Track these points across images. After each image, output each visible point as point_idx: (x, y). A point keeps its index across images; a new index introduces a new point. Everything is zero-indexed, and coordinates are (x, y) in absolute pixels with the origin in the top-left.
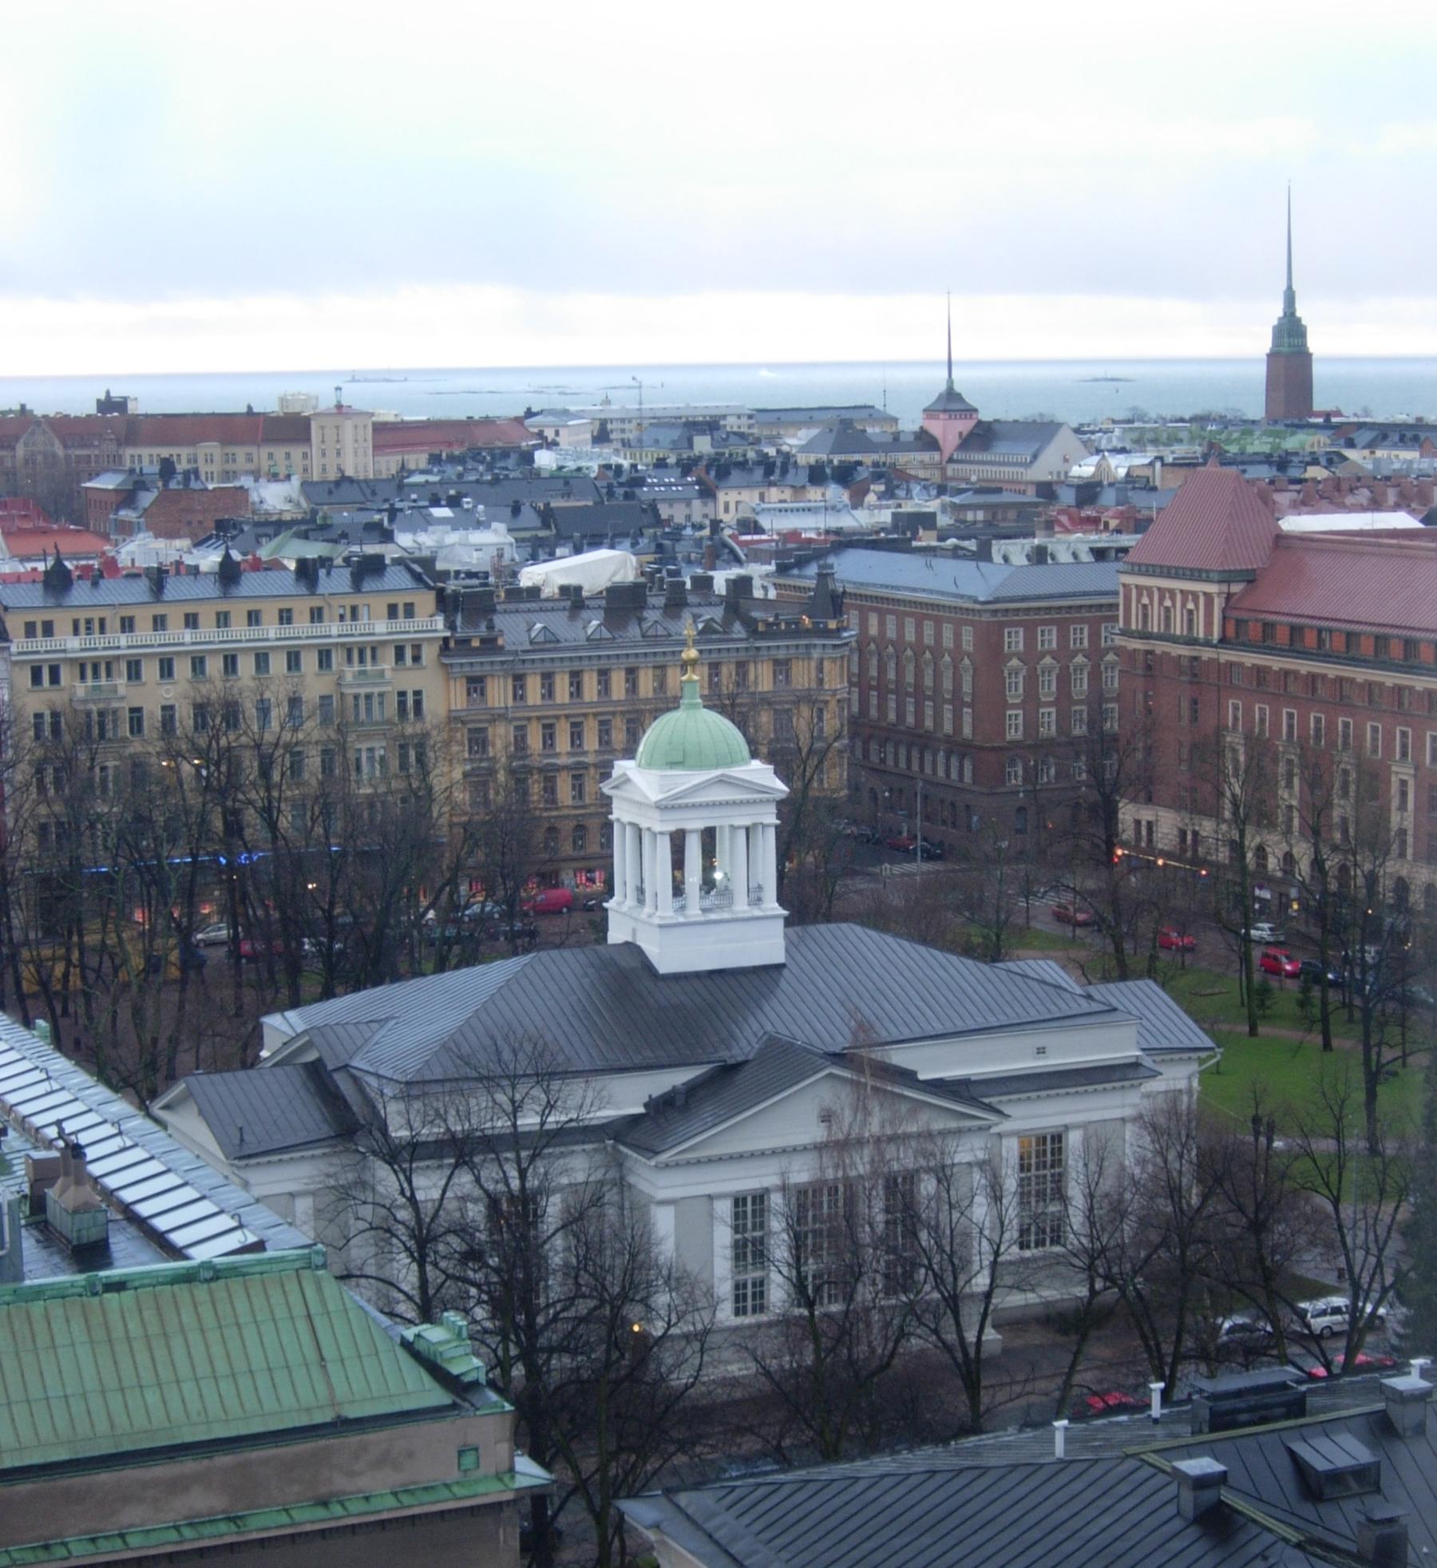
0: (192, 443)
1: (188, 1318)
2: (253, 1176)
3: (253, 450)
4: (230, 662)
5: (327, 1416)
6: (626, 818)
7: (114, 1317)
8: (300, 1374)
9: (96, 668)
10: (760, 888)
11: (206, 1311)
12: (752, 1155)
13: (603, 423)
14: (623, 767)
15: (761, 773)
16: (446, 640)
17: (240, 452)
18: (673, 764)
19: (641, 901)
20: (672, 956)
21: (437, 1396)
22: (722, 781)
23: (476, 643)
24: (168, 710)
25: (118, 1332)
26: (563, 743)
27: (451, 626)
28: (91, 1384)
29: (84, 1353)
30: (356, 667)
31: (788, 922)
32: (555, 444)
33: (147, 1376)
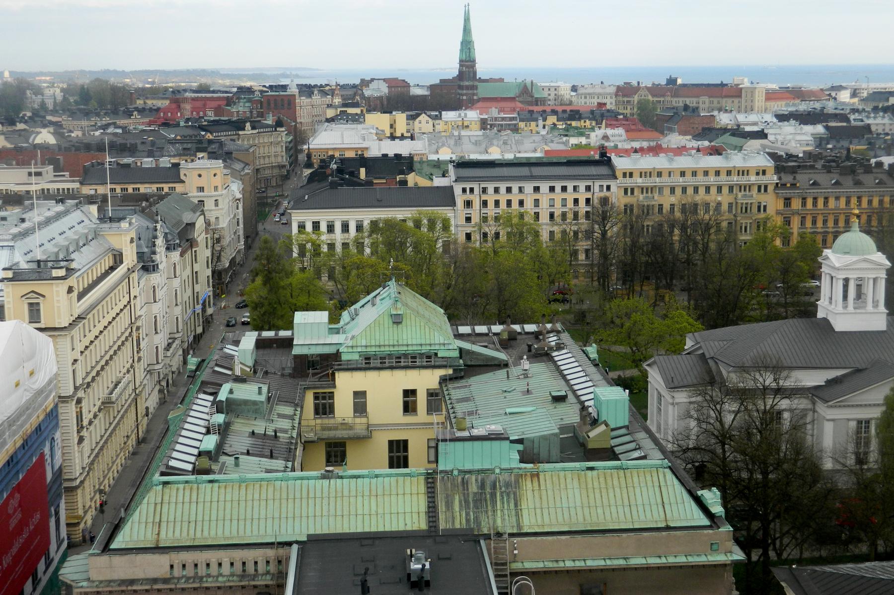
0: (698, 97)
1: (616, 482)
2: (676, 395)
3: (720, 99)
4: (696, 190)
5: (663, 525)
6: (827, 271)
7: (589, 480)
8: (654, 507)
9: (647, 189)
10: (878, 301)
11: (622, 480)
12: (866, 405)
13: (855, 90)
14: (827, 252)
15: (881, 258)
16: (777, 184)
17: (715, 100)
18: (846, 253)
19: (831, 303)
20: (841, 324)
21: (706, 522)
22: (866, 260)
23: (788, 185)
24: (672, 205)
25: (590, 486)
26: (820, 224)
27: (780, 179)
28: (578, 503)
29: (577, 492)
30: (743, 193)
31: (888, 315)
32: (835, 99)
33: (599, 503)
